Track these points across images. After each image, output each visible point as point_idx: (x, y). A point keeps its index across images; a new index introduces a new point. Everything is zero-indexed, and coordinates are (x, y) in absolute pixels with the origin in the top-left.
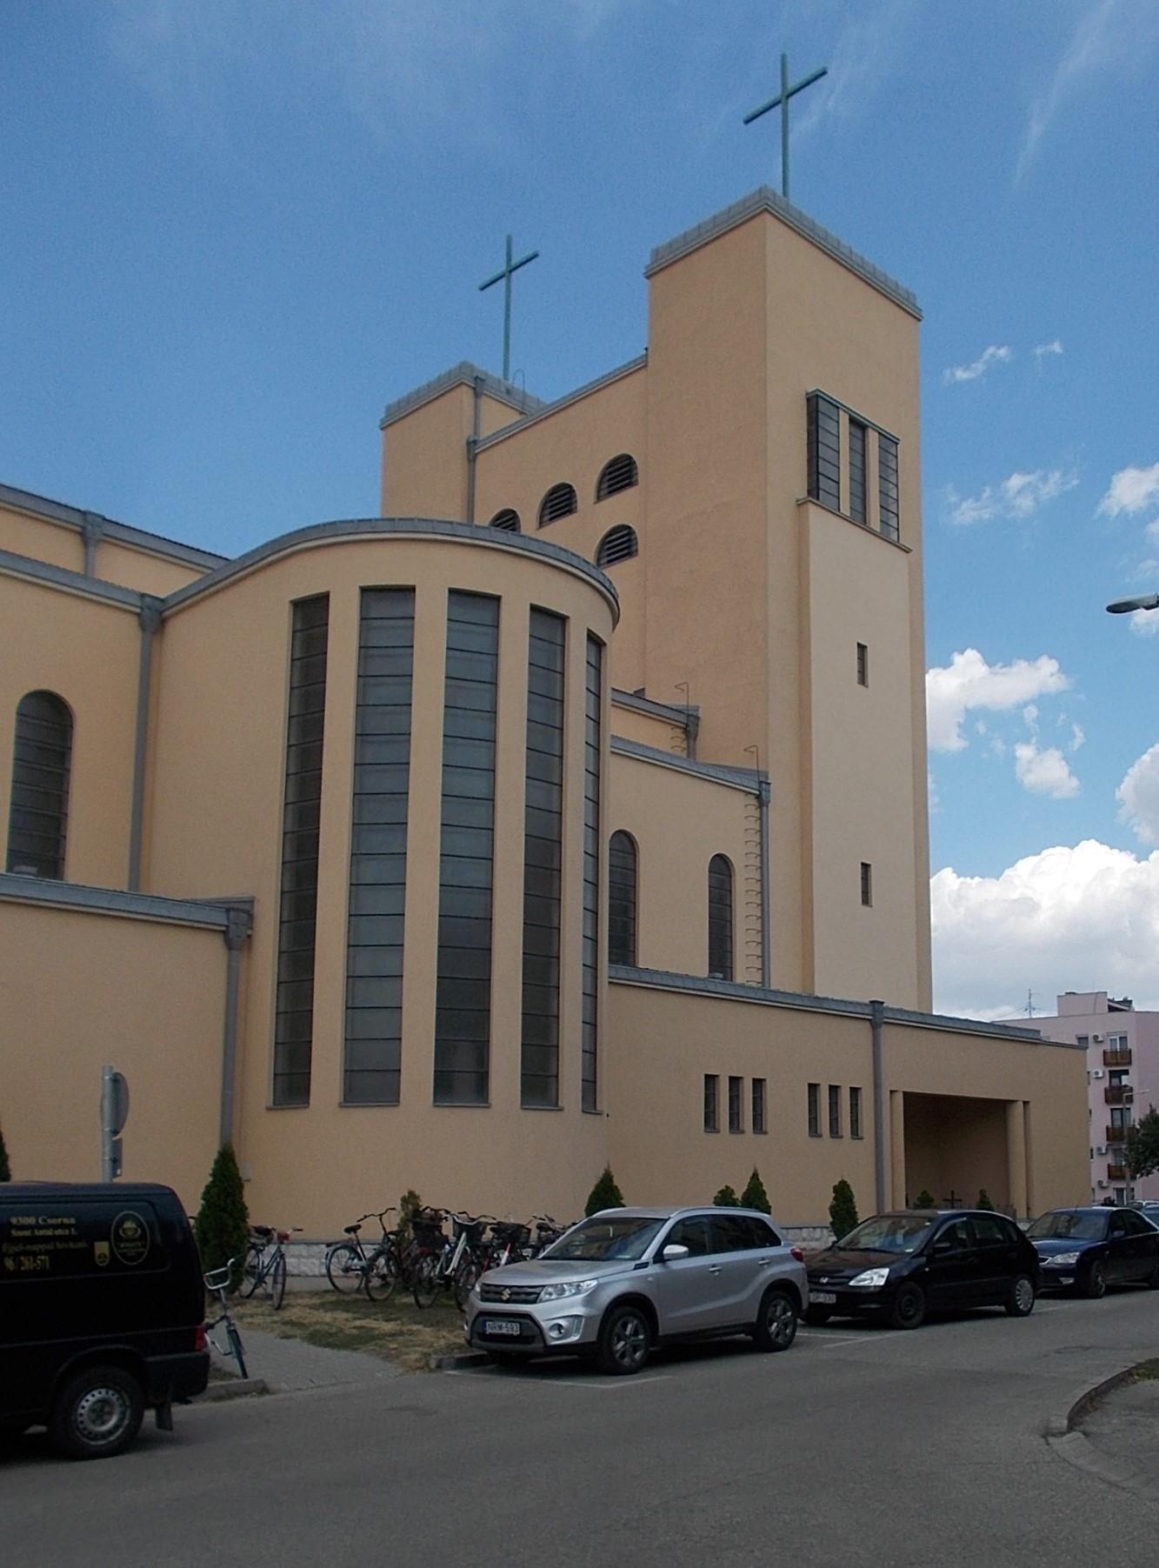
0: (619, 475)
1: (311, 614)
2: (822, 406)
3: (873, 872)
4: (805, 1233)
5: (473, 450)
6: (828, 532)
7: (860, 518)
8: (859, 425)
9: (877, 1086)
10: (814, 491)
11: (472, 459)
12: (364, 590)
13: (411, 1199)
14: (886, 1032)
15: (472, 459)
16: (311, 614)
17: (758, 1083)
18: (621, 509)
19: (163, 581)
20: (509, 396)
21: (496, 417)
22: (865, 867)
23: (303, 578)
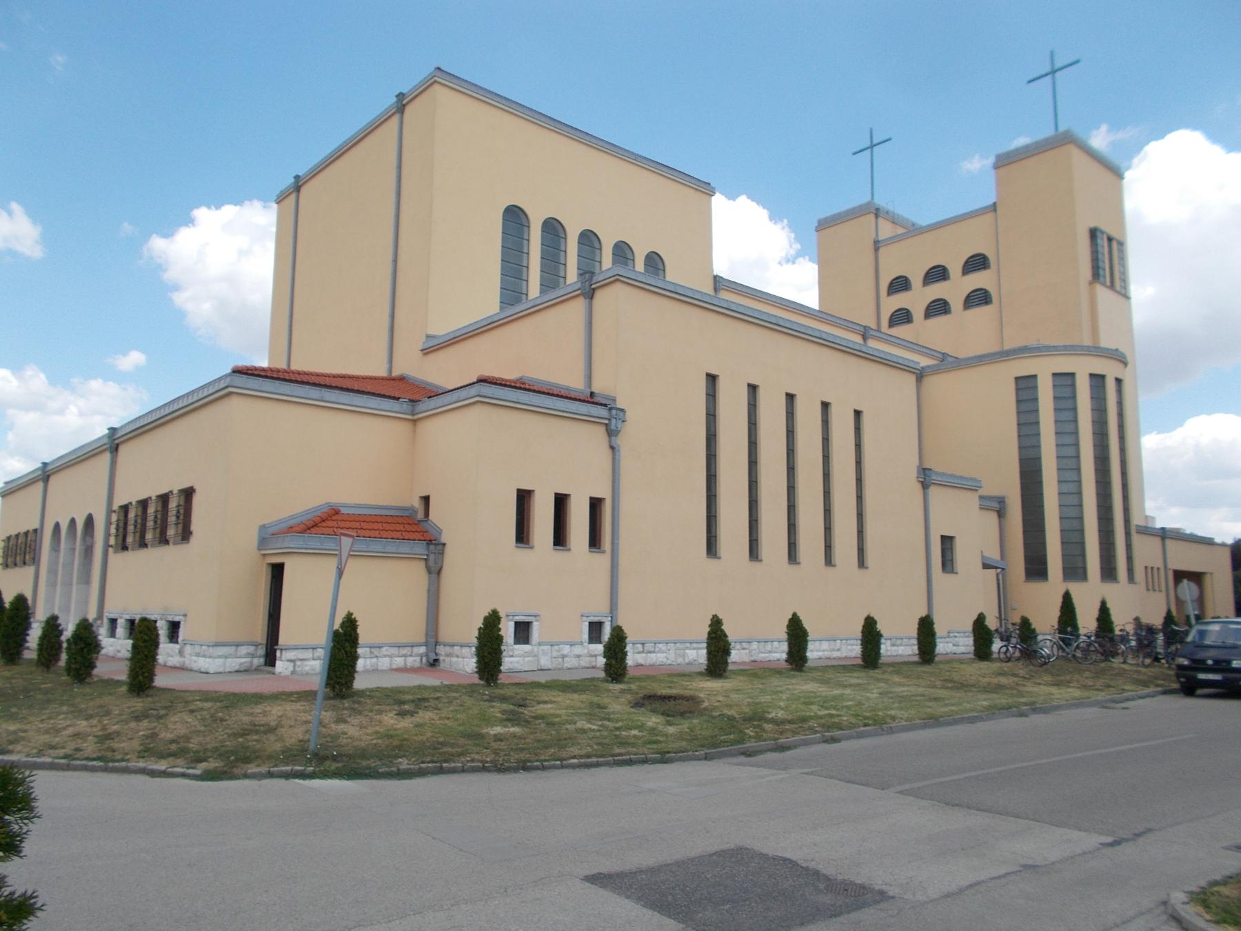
0: (977, 263)
1: (1026, 385)
2: (1098, 234)
3: (762, 394)
4: (769, 646)
5: (877, 245)
6: (1102, 292)
7: (1112, 286)
8: (1110, 239)
9: (1165, 567)
10: (1096, 274)
11: (876, 250)
12: (1054, 375)
13: (1137, 619)
14: (1168, 542)
15: (876, 250)
16: (1026, 385)
17: (523, 535)
18: (979, 280)
19: (924, 362)
20: (894, 220)
21: (886, 230)
22: (753, 388)
23: (1024, 367)
